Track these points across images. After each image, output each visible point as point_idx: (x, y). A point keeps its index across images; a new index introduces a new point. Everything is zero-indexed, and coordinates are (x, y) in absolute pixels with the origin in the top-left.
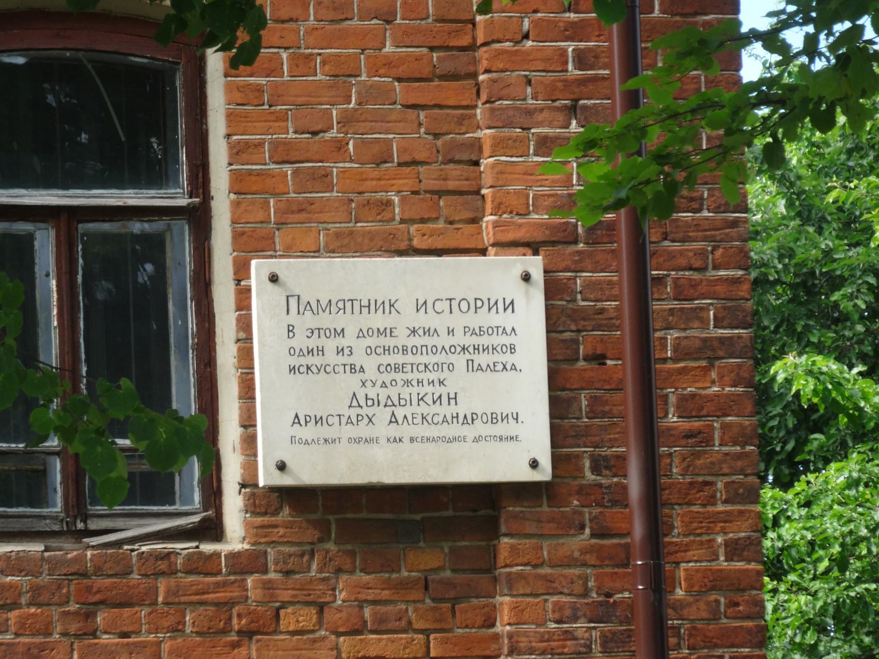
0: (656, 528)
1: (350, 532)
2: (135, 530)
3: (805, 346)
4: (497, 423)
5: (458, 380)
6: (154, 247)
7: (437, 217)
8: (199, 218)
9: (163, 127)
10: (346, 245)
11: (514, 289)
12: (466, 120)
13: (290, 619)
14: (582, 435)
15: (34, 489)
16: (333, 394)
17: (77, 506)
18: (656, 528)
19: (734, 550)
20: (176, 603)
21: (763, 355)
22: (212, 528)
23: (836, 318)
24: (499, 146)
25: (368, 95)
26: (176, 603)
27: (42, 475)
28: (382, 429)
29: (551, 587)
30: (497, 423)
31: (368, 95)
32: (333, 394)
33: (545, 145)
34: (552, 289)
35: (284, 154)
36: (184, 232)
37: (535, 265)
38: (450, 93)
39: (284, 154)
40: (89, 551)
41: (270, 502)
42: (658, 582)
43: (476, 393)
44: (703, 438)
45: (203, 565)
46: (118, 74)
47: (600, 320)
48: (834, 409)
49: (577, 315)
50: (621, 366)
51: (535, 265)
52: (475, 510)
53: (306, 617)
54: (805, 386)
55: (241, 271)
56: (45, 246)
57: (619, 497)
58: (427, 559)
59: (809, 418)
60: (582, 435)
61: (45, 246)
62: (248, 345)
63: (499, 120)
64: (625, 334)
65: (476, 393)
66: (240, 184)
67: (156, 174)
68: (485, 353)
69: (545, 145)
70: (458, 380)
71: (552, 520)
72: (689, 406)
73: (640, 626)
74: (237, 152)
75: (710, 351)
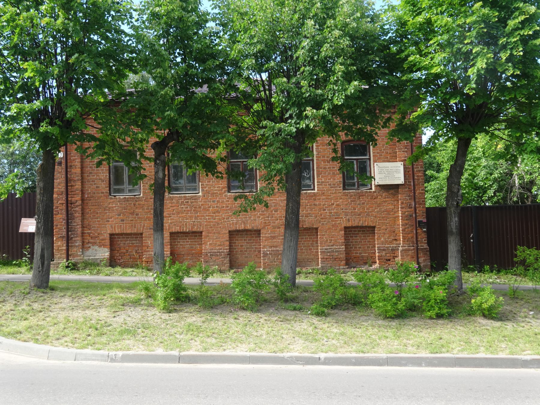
0: (414, 190)
1: (384, 189)
2: (364, 189)
3: (430, 169)
4: (399, 178)
5: (395, 174)
6: (365, 162)
7: (393, 158)
8: (370, 159)
9: (366, 151)
10: (384, 161)
11: (400, 165)
12: (395, 149)
13: (379, 197)
14: (407, 179)
15: (354, 185)
16: (383, 176)
17: (358, 187)
18: (414, 190)
19: (422, 190)
20: (368, 196)
21: (425, 171)
22: (371, 189)
23: (433, 167)
24: (399, 152)
25: (386, 147)
26: (368, 196)
27: (355, 184)
28: (388, 179)
29: (404, 194)
30: (399, 178)
31: (386, 147)
32: (383, 176)
33: (403, 151)
34: (404, 165)
35: (378, 153)
36: (368, 161)
37: (402, 163)
38: (394, 147)
39: (378, 153)
40: (359, 191)
41: (377, 186)
42: (414, 193)
43: (397, 175)
44: (419, 179)
45: (370, 192)
46: (361, 146)
47: (408, 168)
48: (433, 176)
49: (407, 168)
50: (411, 172)
51: (402, 163)
52: (397, 186)
53: (380, 197)
54: (429, 174)
55: (374, 164)
56: (355, 162)
57: (411, 185)
58: (392, 191)
59: (431, 177)
60: (407, 179)
61: (355, 162)
62: (454, 222)
63: (399, 149)
64: (411, 169)
65: (397, 175)
66: (374, 156)
67: (365, 155)
68: (397, 171)
69: (403, 151)
70: (395, 174)
71: (29, 149)
72: (418, 176)
73: (413, 198)
74: (373, 153)
75: (419, 171)
